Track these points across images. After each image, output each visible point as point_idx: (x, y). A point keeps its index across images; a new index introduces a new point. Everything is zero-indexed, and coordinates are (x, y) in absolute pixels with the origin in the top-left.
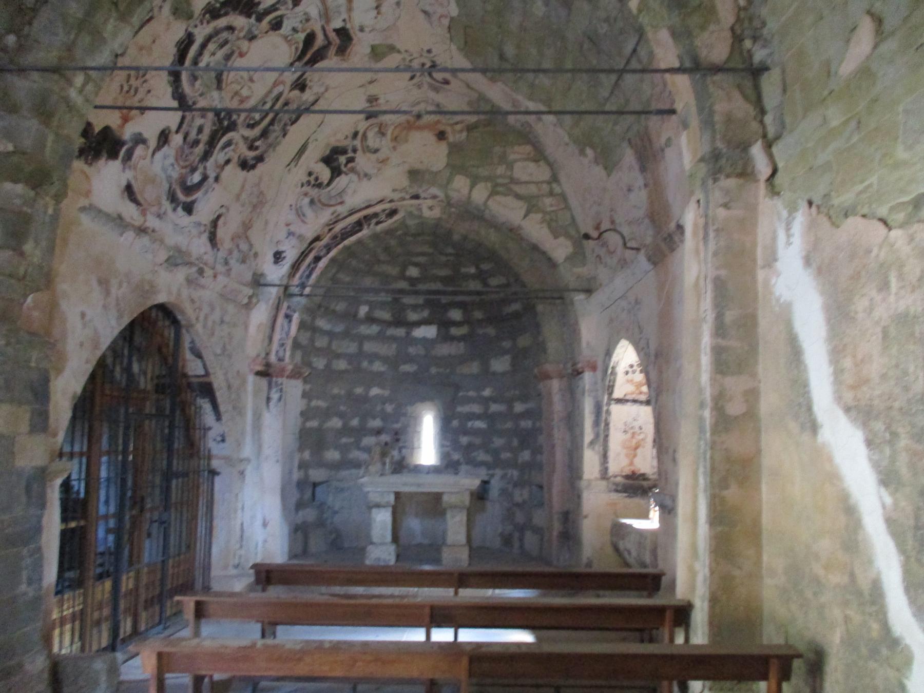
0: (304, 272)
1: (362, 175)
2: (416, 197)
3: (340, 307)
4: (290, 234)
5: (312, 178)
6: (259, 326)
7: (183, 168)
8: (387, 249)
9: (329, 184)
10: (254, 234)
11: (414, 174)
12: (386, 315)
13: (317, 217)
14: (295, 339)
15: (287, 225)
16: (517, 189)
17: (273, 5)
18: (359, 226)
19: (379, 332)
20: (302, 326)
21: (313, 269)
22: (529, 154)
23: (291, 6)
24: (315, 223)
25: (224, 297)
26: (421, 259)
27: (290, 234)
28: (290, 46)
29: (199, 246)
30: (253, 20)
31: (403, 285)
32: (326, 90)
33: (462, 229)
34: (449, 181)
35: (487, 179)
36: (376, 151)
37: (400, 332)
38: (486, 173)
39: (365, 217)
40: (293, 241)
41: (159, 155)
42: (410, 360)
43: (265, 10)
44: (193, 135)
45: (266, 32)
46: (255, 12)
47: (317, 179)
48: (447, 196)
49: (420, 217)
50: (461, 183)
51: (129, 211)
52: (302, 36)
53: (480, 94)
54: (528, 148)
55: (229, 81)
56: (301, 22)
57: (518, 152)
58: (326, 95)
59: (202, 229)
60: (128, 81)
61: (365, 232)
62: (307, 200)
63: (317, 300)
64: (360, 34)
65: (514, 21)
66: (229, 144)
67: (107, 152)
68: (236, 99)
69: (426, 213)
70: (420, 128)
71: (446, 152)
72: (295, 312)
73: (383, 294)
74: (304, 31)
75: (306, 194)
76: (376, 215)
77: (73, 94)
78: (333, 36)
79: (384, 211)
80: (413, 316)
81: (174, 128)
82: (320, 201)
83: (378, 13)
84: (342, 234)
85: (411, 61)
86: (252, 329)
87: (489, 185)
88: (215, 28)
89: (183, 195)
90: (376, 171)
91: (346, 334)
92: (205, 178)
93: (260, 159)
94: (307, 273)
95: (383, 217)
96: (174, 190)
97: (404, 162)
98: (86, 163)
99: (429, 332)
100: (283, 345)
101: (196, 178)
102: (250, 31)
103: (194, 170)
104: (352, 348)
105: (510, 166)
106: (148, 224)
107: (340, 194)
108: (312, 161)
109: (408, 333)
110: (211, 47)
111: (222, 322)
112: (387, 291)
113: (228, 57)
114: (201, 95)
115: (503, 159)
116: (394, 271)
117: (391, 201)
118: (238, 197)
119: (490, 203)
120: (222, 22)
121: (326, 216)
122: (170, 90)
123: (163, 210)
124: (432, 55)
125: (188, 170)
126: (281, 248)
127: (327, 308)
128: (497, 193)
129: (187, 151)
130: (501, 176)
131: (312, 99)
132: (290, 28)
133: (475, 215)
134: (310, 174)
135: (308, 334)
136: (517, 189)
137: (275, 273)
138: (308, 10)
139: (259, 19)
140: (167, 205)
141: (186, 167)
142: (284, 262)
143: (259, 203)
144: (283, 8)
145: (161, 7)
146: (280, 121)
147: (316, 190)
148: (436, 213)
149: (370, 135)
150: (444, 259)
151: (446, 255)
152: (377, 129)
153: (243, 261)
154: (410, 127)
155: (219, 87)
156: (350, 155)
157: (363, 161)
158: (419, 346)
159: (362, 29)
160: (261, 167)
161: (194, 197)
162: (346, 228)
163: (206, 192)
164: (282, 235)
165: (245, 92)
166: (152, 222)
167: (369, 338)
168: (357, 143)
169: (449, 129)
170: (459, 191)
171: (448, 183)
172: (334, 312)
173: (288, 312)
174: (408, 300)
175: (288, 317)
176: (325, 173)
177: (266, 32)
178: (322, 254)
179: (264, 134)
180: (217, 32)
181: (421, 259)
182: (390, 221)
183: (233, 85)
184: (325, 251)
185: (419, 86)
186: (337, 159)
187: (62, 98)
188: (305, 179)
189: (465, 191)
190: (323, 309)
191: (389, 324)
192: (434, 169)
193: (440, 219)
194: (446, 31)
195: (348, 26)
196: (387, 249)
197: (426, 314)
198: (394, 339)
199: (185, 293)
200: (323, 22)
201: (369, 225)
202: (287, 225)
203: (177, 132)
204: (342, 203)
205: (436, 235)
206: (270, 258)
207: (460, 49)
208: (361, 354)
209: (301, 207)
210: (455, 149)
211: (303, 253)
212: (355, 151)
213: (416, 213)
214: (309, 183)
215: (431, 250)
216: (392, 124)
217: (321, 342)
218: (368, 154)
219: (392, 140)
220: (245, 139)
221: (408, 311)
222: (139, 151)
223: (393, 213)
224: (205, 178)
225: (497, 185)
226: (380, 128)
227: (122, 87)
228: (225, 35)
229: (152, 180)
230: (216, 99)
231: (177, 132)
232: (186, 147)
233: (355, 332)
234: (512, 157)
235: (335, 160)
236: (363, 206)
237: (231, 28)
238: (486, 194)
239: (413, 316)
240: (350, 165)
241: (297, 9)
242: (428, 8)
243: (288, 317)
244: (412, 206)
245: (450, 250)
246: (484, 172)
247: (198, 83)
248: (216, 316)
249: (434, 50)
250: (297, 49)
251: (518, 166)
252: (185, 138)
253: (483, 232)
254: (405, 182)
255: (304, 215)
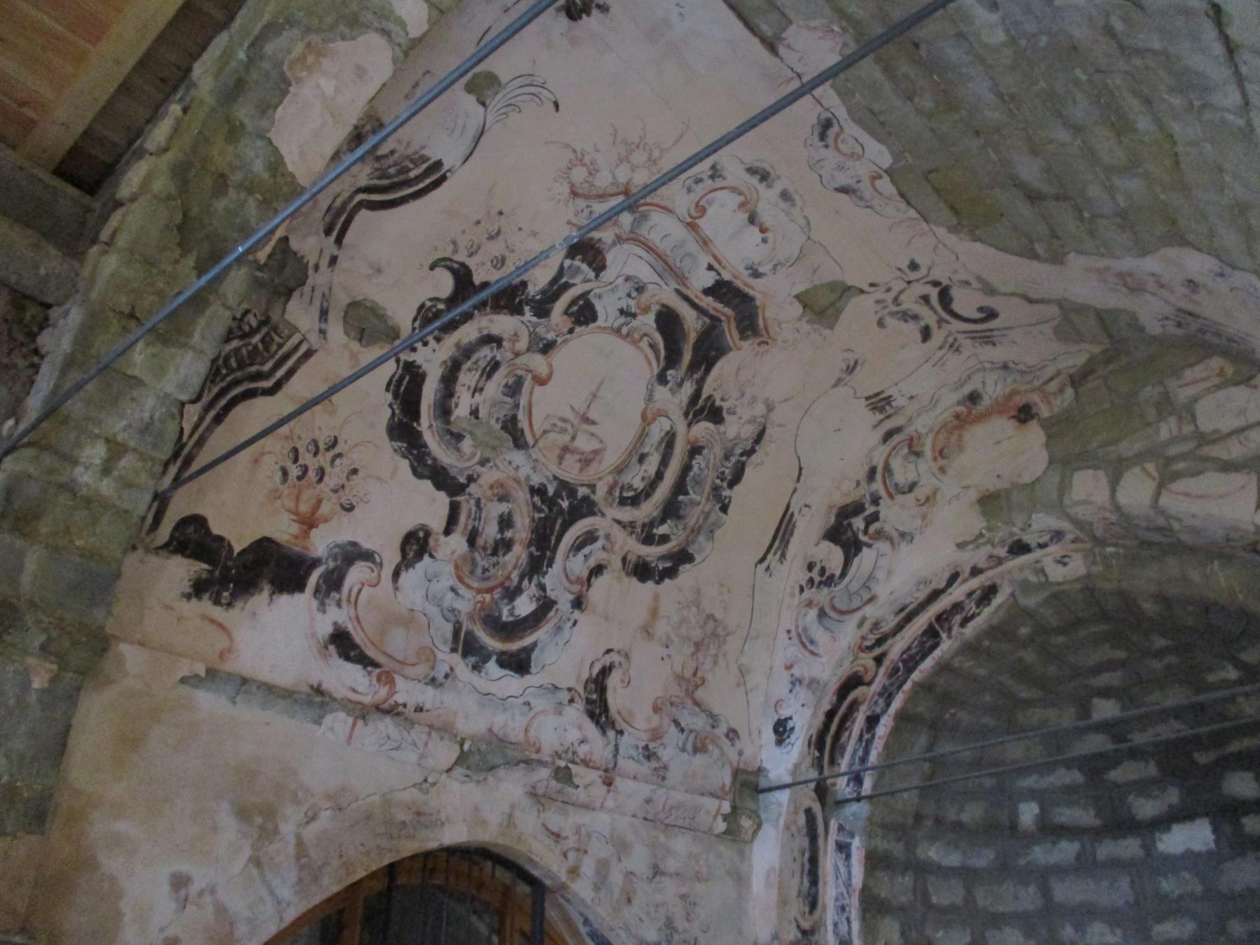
0: (855, 751)
1: (895, 535)
2: (1019, 548)
3: (972, 813)
4: (796, 682)
5: (815, 574)
6: (768, 874)
7: (479, 591)
8: (1022, 673)
9: (844, 574)
10: (718, 694)
11: (989, 502)
12: (1084, 816)
13: (834, 639)
14: (865, 890)
15: (789, 667)
16: (1216, 451)
17: (555, 280)
18: (932, 635)
19: (1078, 857)
20: (874, 861)
21: (869, 743)
22: (1221, 372)
23: (592, 275)
24: (835, 653)
25: (660, 822)
26: (1111, 678)
27: (796, 682)
28: (635, 343)
29: (565, 728)
30: (528, 315)
31: (1097, 743)
32: (770, 409)
33: (1148, 579)
34: (1064, 487)
35: (1140, 458)
36: (912, 487)
37: (1129, 847)
38: (1138, 446)
39: (939, 618)
40: (803, 694)
41: (407, 578)
42: (1171, 908)
43: (543, 292)
44: (490, 532)
45: (571, 331)
46: (529, 301)
47: (823, 571)
48: (1076, 522)
49: (1048, 583)
50: (1088, 487)
51: (346, 678)
52: (648, 322)
53: (1060, 303)
54: (1216, 362)
55: (538, 432)
56: (629, 295)
57: (1193, 381)
58: (774, 416)
59: (565, 696)
60: (296, 460)
61: (947, 646)
62: (813, 613)
63: (908, 800)
64: (758, 283)
65: (978, 88)
66: (589, 538)
67: (272, 583)
68: (570, 459)
69: (1056, 573)
70: (980, 418)
71: (1043, 439)
72: (852, 836)
73: (1061, 772)
74: (646, 310)
75: (810, 604)
76: (957, 607)
77: (85, 477)
78: (708, 302)
79: (970, 595)
80: (1146, 808)
81: (437, 522)
82: (834, 608)
83: (763, 230)
84: (905, 662)
85: (896, 301)
86: (760, 885)
87: (1150, 467)
88: (457, 345)
89: (500, 640)
90: (918, 522)
91: (1004, 870)
92: (546, 606)
93: (683, 557)
94: (860, 753)
95: (971, 607)
96: (469, 634)
97: (967, 487)
98: (217, 602)
99: (1193, 837)
100: (843, 908)
101: (524, 606)
102: (534, 338)
103: (512, 594)
104: (1028, 898)
105: (1188, 412)
106: (399, 698)
107: (866, 586)
108: (809, 541)
109: (1148, 848)
110: (467, 378)
111: (657, 871)
112: (1068, 764)
113: (514, 389)
114: (483, 463)
115: (1166, 405)
116: (1066, 718)
117: (975, 572)
118: (647, 631)
119: (1164, 501)
120: (468, 333)
121: (849, 633)
122: (405, 464)
123: (442, 670)
124: (923, 271)
125: (497, 594)
126: (784, 713)
127: (938, 821)
128: (1177, 476)
129: (482, 562)
130: (1172, 441)
131: (749, 432)
132: (613, 313)
133: (1158, 541)
134: (810, 567)
135: (908, 880)
136: (1216, 451)
137: (782, 762)
138: (629, 271)
139: (542, 310)
140: (449, 659)
141: (490, 591)
142: (793, 737)
143: (710, 636)
144: (577, 280)
145: (322, 332)
146: (698, 483)
147: (825, 590)
148: (1077, 567)
149: (896, 464)
150: (1157, 665)
151: (1160, 654)
152: (906, 450)
153: (699, 749)
154: (961, 422)
155: (519, 442)
156: (870, 509)
157: (894, 514)
158: (1186, 875)
159: (756, 274)
160: (687, 573)
161: (527, 641)
162: (909, 648)
163: (559, 629)
164: (781, 686)
165: (584, 444)
166: (407, 692)
167: (1060, 871)
168: (878, 486)
169: (1036, 398)
170: (1086, 502)
171: (1061, 497)
172: (959, 825)
173: (841, 838)
174: (1122, 774)
175: (843, 848)
176: (833, 556)
177: (571, 331)
178: (878, 710)
179: (671, 510)
180: (467, 352)
181: (1111, 678)
182: (987, 611)
183: (551, 436)
184: (881, 702)
185: (955, 348)
186: (850, 525)
187: (61, 486)
188: (803, 577)
189: (1101, 495)
190: (929, 823)
191: (1097, 834)
192: (1027, 479)
193: (1088, 576)
194: (903, 205)
195: (726, 276)
196: (1022, 673)
197: (1173, 796)
198: (1116, 864)
199: (528, 822)
200: (674, 285)
201: (950, 630)
202: (789, 667)
203: (447, 532)
204: (871, 599)
205: (1102, 615)
206: (769, 736)
207: (953, 229)
208: (1050, 911)
209: (805, 629)
210: (1056, 429)
211: (830, 715)
212: (876, 500)
213: (1033, 579)
214: (811, 581)
215: (1120, 654)
216: (931, 430)
217: (946, 894)
218: (899, 498)
219: (935, 459)
220: (628, 526)
221: (1131, 798)
222: (357, 574)
223: (989, 592)
224: (546, 606)
225: (1170, 461)
226: (910, 446)
227: (285, 473)
228: (486, 353)
229: (408, 620)
230: (517, 466)
231: (447, 532)
232: (477, 555)
233: (1022, 862)
234: (1183, 395)
235: (847, 530)
236: (922, 595)
237: (491, 340)
238: (1149, 487)
239: (1146, 808)
240: (872, 529)
241: (607, 275)
242: (843, 179)
243: (843, 848)
244: (1021, 569)
245: (1160, 642)
246: (1127, 448)
247: (467, 445)
248: (639, 860)
249: (919, 261)
250: (653, 346)
251: (1200, 408)
252: (472, 539)
253: (1195, 575)
254: (977, 523)
255: (812, 642)
